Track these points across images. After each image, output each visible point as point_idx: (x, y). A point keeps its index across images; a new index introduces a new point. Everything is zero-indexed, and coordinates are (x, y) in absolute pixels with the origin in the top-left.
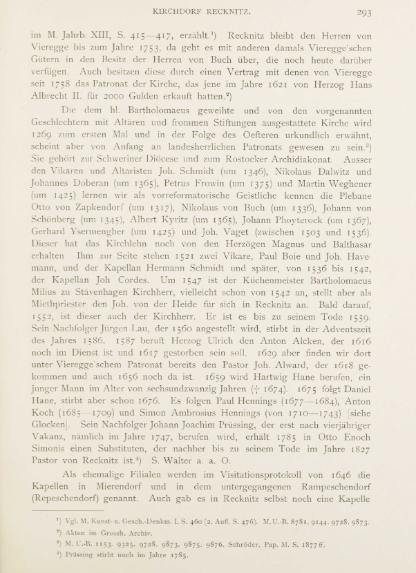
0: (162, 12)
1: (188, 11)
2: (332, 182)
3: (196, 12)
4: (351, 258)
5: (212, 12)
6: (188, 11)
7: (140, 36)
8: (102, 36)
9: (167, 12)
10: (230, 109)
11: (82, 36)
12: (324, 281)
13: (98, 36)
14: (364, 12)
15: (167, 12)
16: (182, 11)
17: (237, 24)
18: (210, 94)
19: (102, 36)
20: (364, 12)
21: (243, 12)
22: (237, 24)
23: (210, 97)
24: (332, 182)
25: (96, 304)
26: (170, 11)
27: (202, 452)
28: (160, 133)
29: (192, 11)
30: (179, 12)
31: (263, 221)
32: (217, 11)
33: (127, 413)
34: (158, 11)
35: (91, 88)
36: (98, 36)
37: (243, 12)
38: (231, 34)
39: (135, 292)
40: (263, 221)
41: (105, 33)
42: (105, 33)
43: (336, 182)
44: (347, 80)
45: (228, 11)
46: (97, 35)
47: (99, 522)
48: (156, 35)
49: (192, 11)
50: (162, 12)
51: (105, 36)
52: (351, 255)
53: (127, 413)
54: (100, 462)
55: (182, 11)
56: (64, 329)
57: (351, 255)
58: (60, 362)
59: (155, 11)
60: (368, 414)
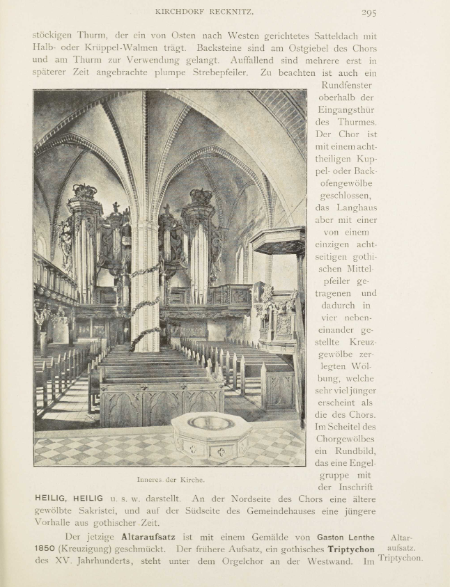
1: (191, 12)
2: (231, 34)
3: (199, 12)
4: (37, 48)
6: (191, 12)
9: (169, 12)
14: (369, 12)
16: (185, 12)
17: (240, 24)
20: (369, 12)
21: (246, 12)
22: (240, 24)
24: (231, 34)
25: (338, 49)
26: (173, 12)
28: (372, 59)
29: (195, 12)
30: (182, 12)
32: (220, 12)
33: (256, 49)
34: (161, 12)
37: (246, 12)
38: (325, 83)
39: (87, 47)
43: (130, 46)
44: (249, 543)
45: (231, 11)
49: (195, 12)
52: (36, 45)
53: (256, 49)
54: (215, 50)
55: (185, 12)
56: (206, 49)
57: (36, 45)
59: (157, 12)
60: (35, 60)
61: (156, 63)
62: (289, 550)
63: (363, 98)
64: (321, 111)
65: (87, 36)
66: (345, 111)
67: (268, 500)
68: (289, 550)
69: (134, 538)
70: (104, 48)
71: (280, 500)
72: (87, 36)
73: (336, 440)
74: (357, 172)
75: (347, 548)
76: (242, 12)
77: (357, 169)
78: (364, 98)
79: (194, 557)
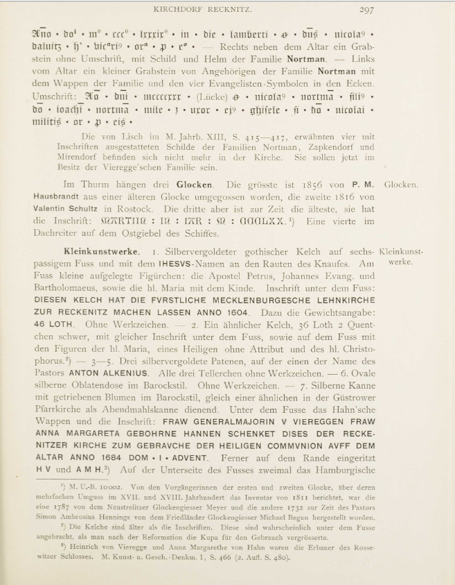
0: (163, 10)
1: (189, 9)
3: (197, 10)
5: (213, 10)
6: (189, 9)
7: (255, 138)
8: (217, 138)
9: (168, 9)
10: (201, 208)
11: (198, 138)
12: (48, 288)
13: (213, 138)
15: (168, 9)
16: (183, 9)
18: (260, 347)
19: (217, 138)
20: (367, 10)
21: (244, 10)
23: (260, 350)
27: (127, 75)
30: (180, 10)
31: (180, 548)
32: (218, 9)
35: (165, 521)
36: (213, 138)
40: (180, 548)
41: (220, 136)
42: (220, 136)
46: (213, 137)
47: (95, 252)
48: (271, 137)
50: (163, 10)
51: (220, 138)
55: (183, 9)
58: (106, 165)
61: (102, 389)
62: (185, 362)
63: (262, 411)
64: (212, 85)
65: (90, 185)
66: (349, 314)
67: (332, 137)
68: (253, 253)
69: (320, 48)
70: (71, 84)
71: (247, 265)
72: (90, 185)
73: (177, 362)
74: (147, 387)
75: (335, 70)
76: (240, 10)
77: (147, 384)
78: (366, 362)
79: (358, 142)
